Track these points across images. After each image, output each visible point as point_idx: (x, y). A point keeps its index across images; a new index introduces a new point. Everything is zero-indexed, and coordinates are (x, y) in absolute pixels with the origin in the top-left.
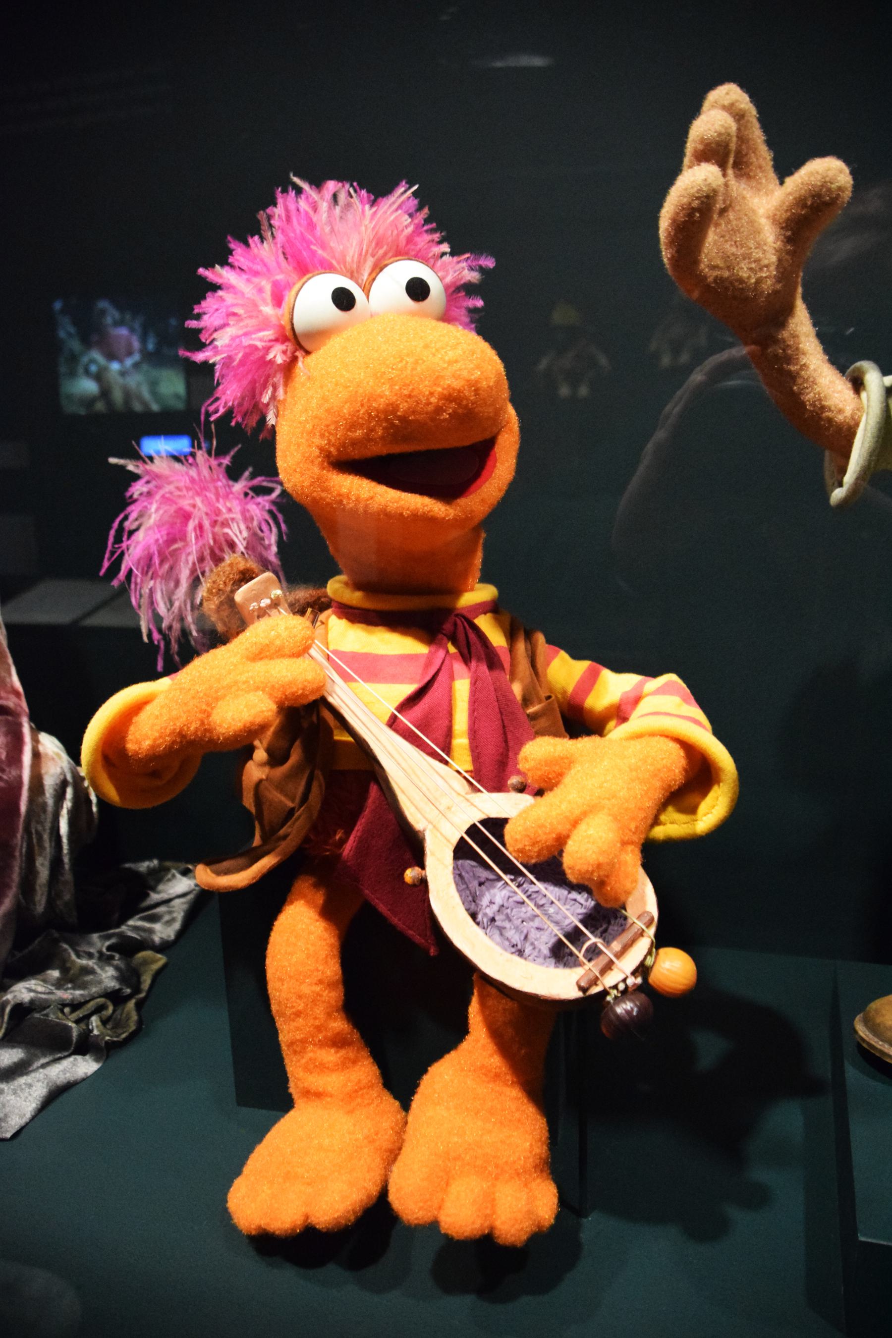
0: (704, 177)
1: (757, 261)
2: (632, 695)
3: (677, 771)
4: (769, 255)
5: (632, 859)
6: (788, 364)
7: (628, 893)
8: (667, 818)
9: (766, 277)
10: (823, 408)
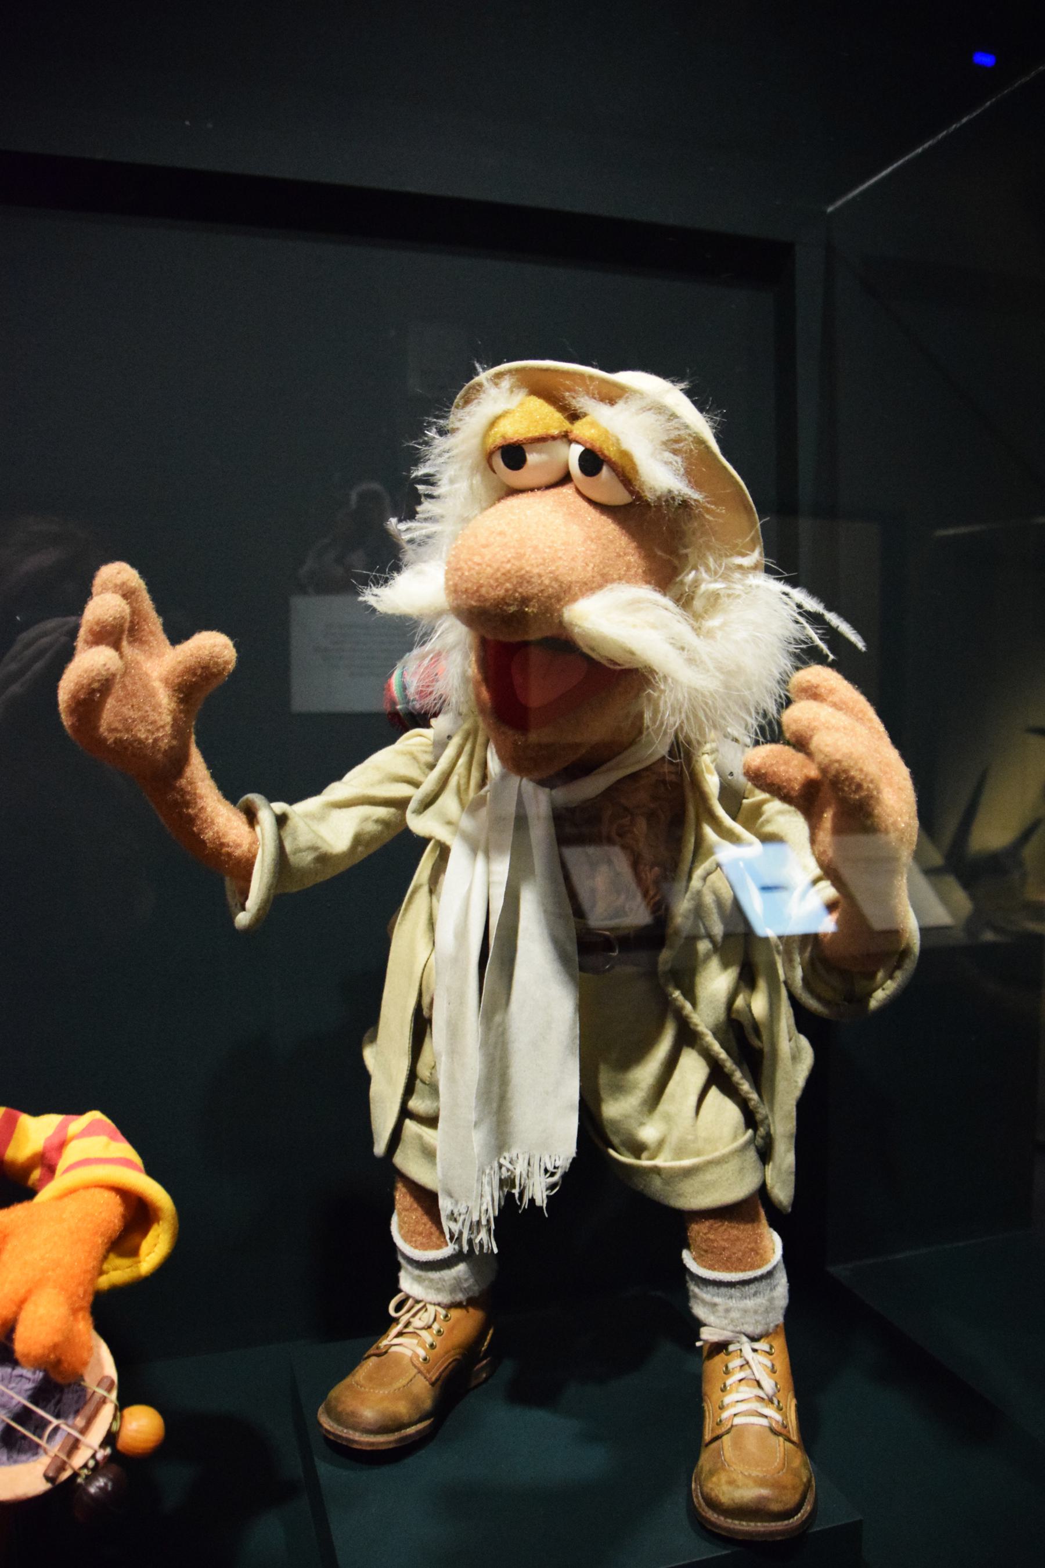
0: (103, 663)
1: (153, 722)
2: (56, 1141)
3: (116, 1221)
4: (164, 716)
5: (84, 1327)
6: (188, 808)
7: (85, 1364)
8: (109, 1267)
9: (163, 736)
10: (222, 845)
